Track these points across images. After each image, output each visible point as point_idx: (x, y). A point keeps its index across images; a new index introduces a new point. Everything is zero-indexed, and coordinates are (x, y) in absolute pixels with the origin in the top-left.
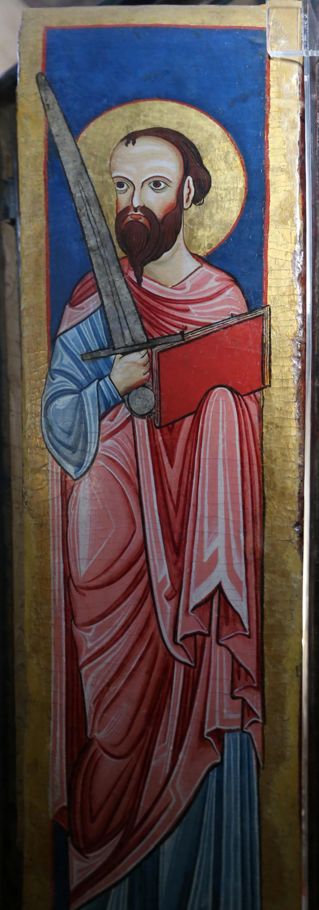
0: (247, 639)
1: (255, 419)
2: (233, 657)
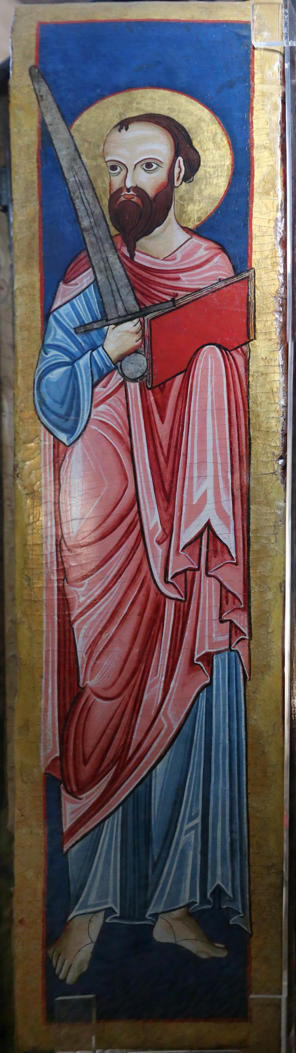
0: (234, 566)
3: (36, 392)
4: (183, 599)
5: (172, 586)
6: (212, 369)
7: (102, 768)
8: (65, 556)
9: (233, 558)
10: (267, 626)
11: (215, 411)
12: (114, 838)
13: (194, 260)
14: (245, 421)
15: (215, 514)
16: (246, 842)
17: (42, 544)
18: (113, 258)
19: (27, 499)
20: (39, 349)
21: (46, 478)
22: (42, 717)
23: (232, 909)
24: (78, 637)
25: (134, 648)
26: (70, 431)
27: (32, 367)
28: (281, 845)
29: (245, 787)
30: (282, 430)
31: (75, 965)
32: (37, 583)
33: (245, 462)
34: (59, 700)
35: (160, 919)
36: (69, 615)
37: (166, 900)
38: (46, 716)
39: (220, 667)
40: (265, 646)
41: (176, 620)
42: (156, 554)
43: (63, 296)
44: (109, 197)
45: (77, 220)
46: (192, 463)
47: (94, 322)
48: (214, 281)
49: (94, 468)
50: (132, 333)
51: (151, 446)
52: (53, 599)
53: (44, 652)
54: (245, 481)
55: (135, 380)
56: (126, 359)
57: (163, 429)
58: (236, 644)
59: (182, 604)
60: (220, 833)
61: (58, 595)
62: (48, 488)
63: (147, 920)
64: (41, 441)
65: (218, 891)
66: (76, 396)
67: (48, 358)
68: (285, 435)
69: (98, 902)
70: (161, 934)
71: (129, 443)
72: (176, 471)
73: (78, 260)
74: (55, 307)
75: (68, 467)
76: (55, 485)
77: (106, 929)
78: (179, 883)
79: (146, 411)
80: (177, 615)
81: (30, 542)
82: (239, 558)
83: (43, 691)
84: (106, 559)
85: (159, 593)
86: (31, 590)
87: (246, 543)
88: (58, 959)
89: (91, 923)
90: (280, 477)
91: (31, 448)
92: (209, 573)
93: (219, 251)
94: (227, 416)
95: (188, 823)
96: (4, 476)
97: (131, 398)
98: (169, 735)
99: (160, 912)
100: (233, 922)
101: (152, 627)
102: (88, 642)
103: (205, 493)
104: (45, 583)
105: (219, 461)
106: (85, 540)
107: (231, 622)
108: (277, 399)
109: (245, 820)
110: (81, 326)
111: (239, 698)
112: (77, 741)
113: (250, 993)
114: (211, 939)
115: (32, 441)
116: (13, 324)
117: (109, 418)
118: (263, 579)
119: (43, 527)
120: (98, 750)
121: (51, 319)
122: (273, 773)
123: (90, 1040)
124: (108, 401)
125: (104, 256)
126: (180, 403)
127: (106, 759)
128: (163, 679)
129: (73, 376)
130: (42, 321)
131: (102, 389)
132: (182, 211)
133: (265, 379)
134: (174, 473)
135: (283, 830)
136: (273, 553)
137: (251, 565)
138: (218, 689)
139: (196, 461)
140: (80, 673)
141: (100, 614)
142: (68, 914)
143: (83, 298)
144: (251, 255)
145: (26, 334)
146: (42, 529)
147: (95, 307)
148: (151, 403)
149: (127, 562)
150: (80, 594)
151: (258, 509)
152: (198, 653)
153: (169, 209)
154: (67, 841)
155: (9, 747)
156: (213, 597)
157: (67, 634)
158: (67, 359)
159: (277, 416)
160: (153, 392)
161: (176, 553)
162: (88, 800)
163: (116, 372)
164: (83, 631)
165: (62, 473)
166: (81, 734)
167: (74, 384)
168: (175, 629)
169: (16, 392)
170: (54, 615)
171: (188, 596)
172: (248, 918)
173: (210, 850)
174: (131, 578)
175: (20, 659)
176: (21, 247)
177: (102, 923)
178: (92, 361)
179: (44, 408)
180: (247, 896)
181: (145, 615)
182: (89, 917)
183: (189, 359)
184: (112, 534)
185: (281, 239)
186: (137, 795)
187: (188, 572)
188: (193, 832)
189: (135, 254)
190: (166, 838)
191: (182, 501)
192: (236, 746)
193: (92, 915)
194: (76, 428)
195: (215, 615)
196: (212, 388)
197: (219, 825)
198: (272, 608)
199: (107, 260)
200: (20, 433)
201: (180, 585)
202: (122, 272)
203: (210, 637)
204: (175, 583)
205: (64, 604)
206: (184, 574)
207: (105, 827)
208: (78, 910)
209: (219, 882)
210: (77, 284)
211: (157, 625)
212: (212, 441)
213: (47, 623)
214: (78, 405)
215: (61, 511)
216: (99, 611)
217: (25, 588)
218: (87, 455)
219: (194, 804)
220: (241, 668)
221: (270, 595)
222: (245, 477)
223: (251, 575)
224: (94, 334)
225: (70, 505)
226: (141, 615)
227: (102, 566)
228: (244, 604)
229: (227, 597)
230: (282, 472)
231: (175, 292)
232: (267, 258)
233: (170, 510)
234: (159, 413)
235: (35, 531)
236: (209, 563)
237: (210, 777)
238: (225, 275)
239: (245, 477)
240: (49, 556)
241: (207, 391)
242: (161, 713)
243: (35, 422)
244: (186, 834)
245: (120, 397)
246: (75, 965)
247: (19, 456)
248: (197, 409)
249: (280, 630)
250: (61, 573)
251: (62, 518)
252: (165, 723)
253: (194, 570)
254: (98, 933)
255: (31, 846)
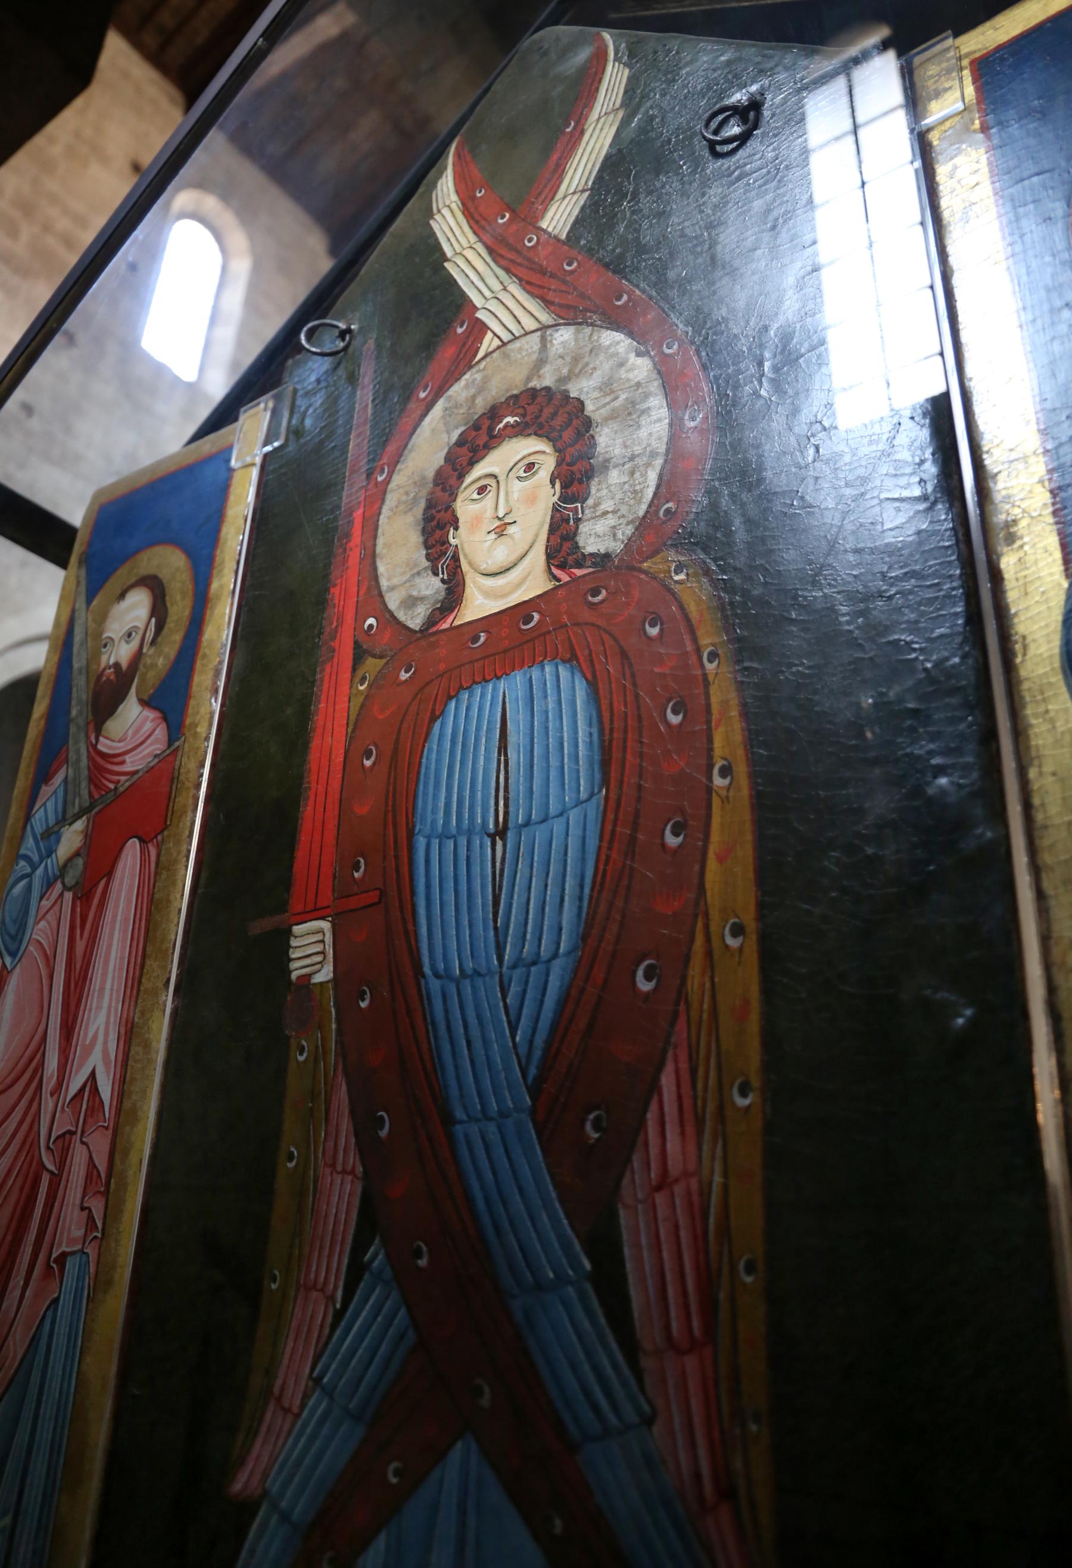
0: (104, 1130)
1: (153, 865)
2: (91, 1157)
195: (78, 1202)
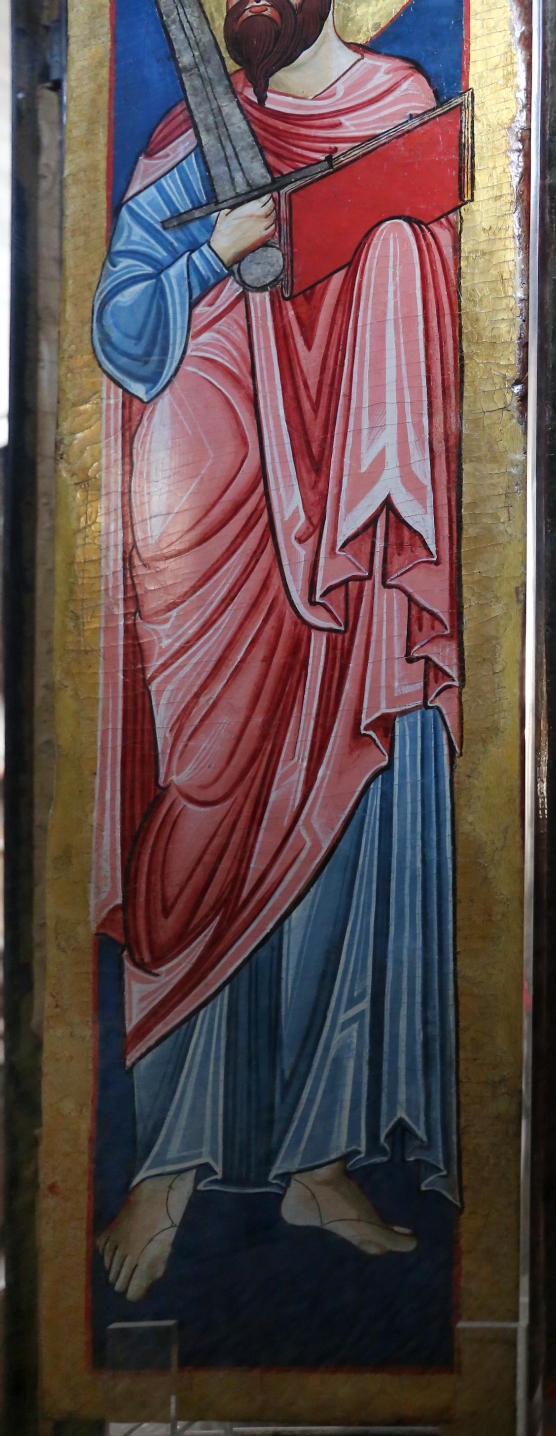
0: (433, 567)
3: (95, 325)
4: (342, 628)
5: (322, 609)
6: (395, 256)
7: (195, 921)
8: (137, 576)
9: (430, 554)
10: (493, 661)
11: (400, 320)
12: (214, 1041)
13: (367, 92)
14: (454, 331)
15: (400, 485)
16: (453, 1041)
17: (100, 559)
18: (230, 108)
19: (76, 491)
20: (103, 260)
21: (108, 456)
22: (94, 840)
23: (425, 1162)
24: (158, 705)
25: (254, 716)
26: (150, 380)
27: (90, 289)
28: (516, 1043)
29: (451, 941)
30: (520, 338)
31: (143, 1267)
32: (89, 623)
33: (453, 396)
34: (123, 811)
35: (293, 1184)
36: (143, 670)
37: (305, 1149)
38: (100, 837)
39: (407, 738)
40: (489, 695)
41: (329, 664)
42: (295, 558)
43: (145, 176)
44: (225, 14)
45: (172, 55)
46: (359, 408)
47: (194, 208)
48: (400, 119)
49: (190, 432)
50: (259, 217)
51: (289, 389)
52: (117, 647)
53: (99, 733)
54: (453, 427)
55: (262, 289)
56: (249, 258)
57: (309, 360)
58: (436, 696)
59: (340, 638)
60: (405, 1026)
61: (126, 638)
62: (113, 470)
63: (269, 1184)
64: (102, 399)
65: (401, 1131)
66: (162, 324)
67: (117, 272)
68: (524, 346)
69: (185, 1154)
70: (295, 1211)
71: (251, 386)
72: (331, 422)
73: (170, 118)
74: (130, 193)
75: (145, 435)
76: (123, 464)
77: (198, 1203)
78: (330, 1116)
79: (281, 333)
80: (330, 656)
81: (80, 558)
82: (442, 553)
83: (97, 796)
84: (208, 574)
85: (299, 621)
86: (79, 635)
87: (455, 527)
88: (114, 1255)
89: (172, 1193)
90: (517, 414)
91: (85, 412)
92: (389, 582)
93: (410, 71)
94: (421, 327)
95: (346, 1011)
96: (39, 459)
97: (256, 317)
98: (315, 859)
99: (294, 1170)
100: (427, 1186)
101: (287, 679)
102: (175, 711)
103: (382, 453)
104: (103, 621)
105: (407, 399)
106: (173, 548)
107: (427, 659)
108: (510, 289)
109: (451, 1001)
110: (172, 217)
111: (441, 787)
112: (153, 877)
113: (459, 1318)
114: (386, 1219)
115: (86, 402)
116: (61, 228)
117: (217, 352)
118: (485, 584)
119: (102, 533)
120: (188, 891)
121: (124, 211)
122: (503, 915)
123: (166, 1403)
124: (216, 326)
125: (214, 106)
126: (339, 315)
127: (202, 906)
128: (305, 764)
129: (157, 295)
130: (108, 218)
131: (207, 308)
132: (347, 18)
133: (489, 261)
134: (328, 426)
135: (521, 1015)
136: (503, 539)
137: (463, 562)
138: (403, 775)
139: (366, 403)
140: (161, 764)
141: (197, 663)
142: (132, 1176)
143: (177, 176)
144: (468, 68)
145: (81, 240)
146: (100, 536)
147: (198, 185)
148: (289, 321)
149: (244, 577)
150: (162, 634)
151: (476, 469)
152: (367, 717)
153: (324, 18)
154: (134, 1047)
155: (38, 891)
156: (396, 621)
157: (140, 701)
158: (149, 270)
159: (511, 316)
160: (293, 304)
161: (330, 554)
162: (171, 976)
163: (231, 279)
164: (166, 695)
165: (137, 444)
166: (160, 866)
167: (159, 307)
168: (327, 679)
169: (62, 328)
170: (117, 672)
171: (351, 624)
172: (456, 1178)
173: (385, 1056)
174: (251, 602)
175: (59, 747)
176: (79, 108)
177: (191, 1191)
178: (191, 267)
179: (108, 348)
180: (454, 1138)
181: (275, 660)
182: (168, 1181)
183: (356, 246)
184: (218, 535)
185: (523, 33)
186: (257, 965)
187: (350, 583)
188: (355, 1026)
189: (267, 97)
190: (306, 1038)
191: (342, 469)
192: (435, 871)
193: (174, 1176)
194: (161, 374)
195: (399, 650)
196: (395, 285)
197: (404, 1012)
198: (501, 631)
199: (220, 111)
200: (67, 391)
201: (337, 607)
202: (244, 125)
203: (390, 688)
204: (328, 603)
205: (134, 653)
206: (343, 588)
207: (199, 1022)
208: (150, 1168)
209: (401, 1114)
210: (167, 155)
211: (296, 674)
212: (395, 369)
213: (106, 685)
214: (166, 338)
215: (134, 505)
216: (194, 660)
217: (70, 632)
218: (180, 413)
219: (358, 976)
220: (445, 736)
221: (497, 610)
222: (453, 420)
223: (464, 578)
224: (194, 227)
225: (149, 493)
226: (268, 660)
227: (201, 586)
228: (451, 627)
229: (420, 619)
230: (520, 405)
231: (333, 145)
232: (496, 67)
233: (321, 485)
234: (303, 334)
235: (88, 540)
236: (389, 566)
237: (388, 927)
238: (421, 108)
239: (453, 420)
240: (111, 578)
241: (387, 292)
242: (300, 822)
243: (93, 371)
244: (342, 1029)
245: (236, 316)
246: (143, 1267)
247: (65, 426)
248: (369, 321)
249: (517, 667)
250: (131, 603)
251: (135, 515)
252: (307, 839)
253: (361, 579)
254: (184, 1208)
255: (71, 1058)
